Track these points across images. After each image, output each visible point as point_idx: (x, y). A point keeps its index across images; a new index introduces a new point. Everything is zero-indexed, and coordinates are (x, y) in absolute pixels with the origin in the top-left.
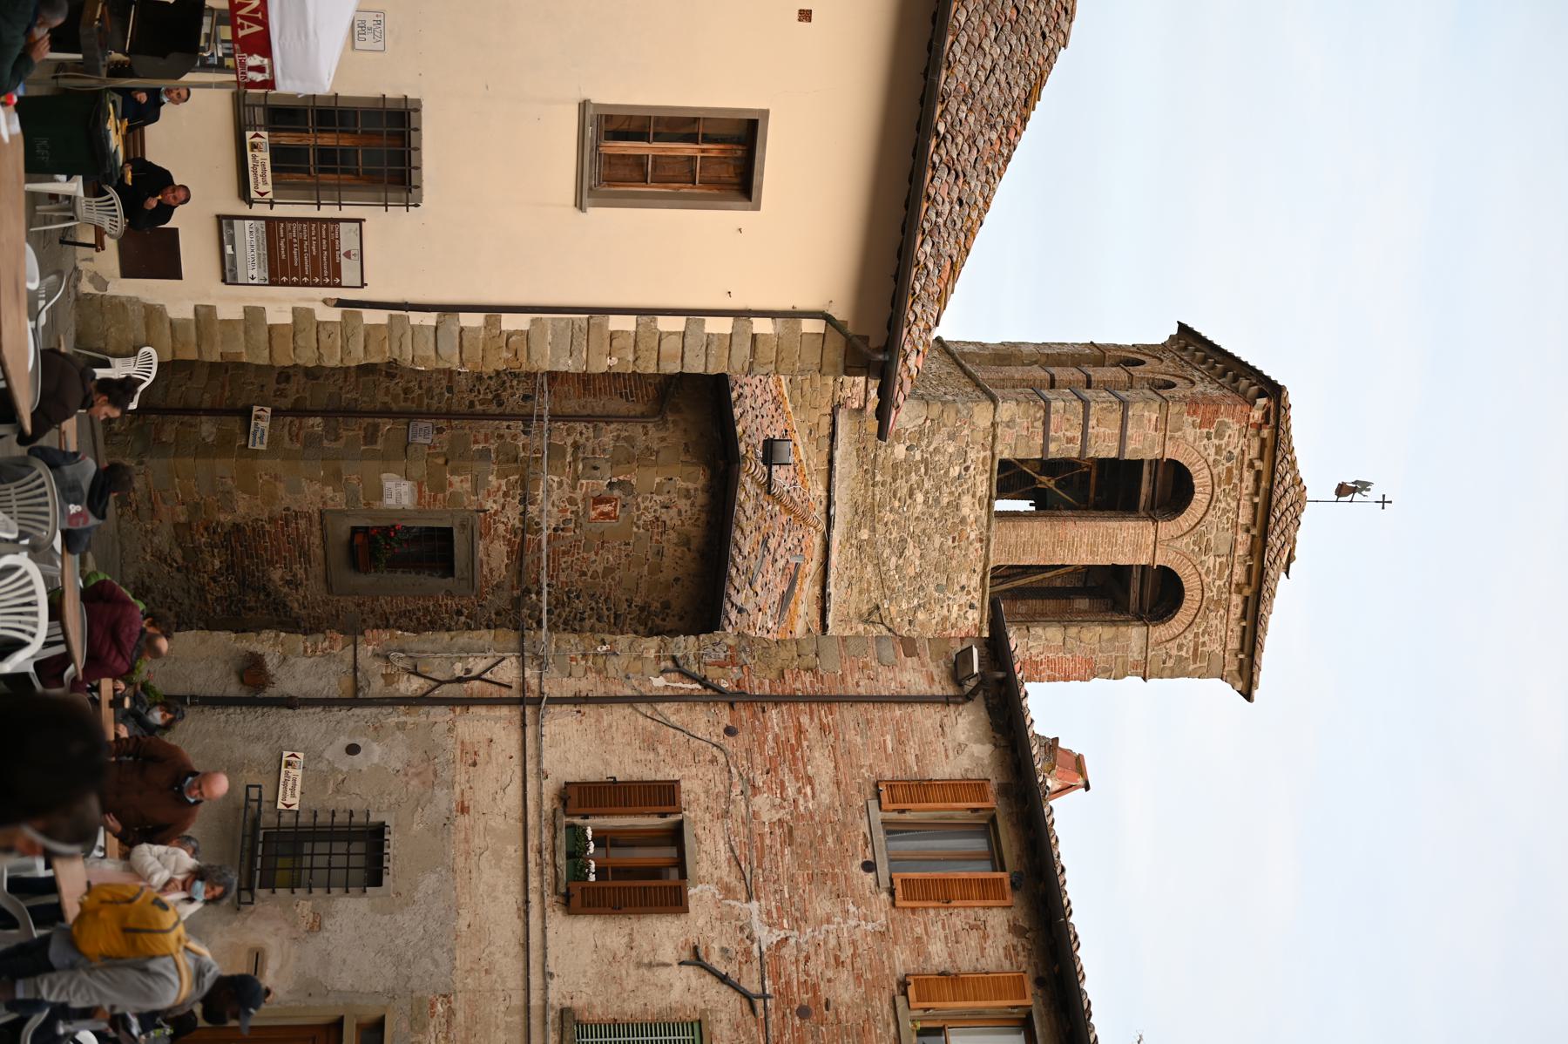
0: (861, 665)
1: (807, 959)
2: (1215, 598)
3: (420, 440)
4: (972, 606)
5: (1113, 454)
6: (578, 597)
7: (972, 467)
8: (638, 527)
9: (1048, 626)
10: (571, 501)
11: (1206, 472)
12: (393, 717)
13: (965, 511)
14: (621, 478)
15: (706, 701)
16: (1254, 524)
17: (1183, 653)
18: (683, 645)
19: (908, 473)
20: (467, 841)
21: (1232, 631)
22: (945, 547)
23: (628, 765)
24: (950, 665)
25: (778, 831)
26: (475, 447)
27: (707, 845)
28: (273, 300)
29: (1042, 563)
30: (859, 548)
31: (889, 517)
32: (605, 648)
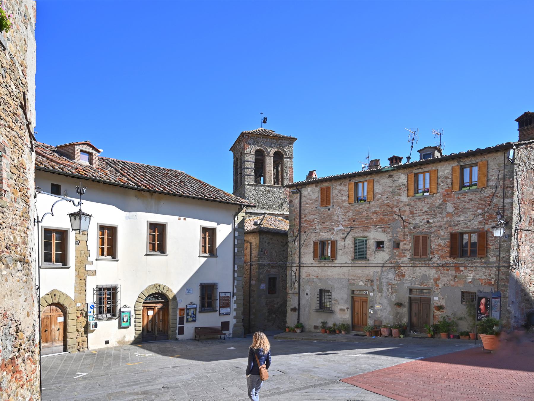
1: (345, 220)
3: (254, 283)
10: (264, 258)
12: (302, 288)
20: (323, 276)
23: (311, 249)
25: (322, 225)
27: (325, 237)
28: (233, 307)
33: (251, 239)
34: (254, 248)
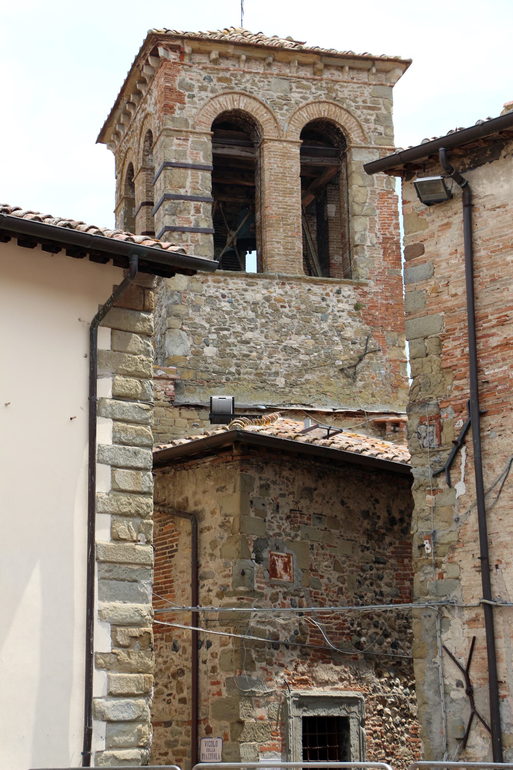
0: (434, 295)
2: (326, 92)
4: (339, 292)
5: (208, 175)
6: (362, 597)
7: (222, 291)
8: (296, 536)
9: (353, 229)
11: (221, 99)
13: (259, 297)
14: (251, 549)
15: (479, 440)
16: (264, 59)
17: (373, 118)
18: (420, 469)
19: (229, 345)
21: (353, 78)
22: (290, 314)
24: (431, 210)
26: (225, 694)
29: (301, 234)
30: (292, 386)
31: (266, 361)
32: (427, 546)
33: (199, 496)
34: (214, 544)
